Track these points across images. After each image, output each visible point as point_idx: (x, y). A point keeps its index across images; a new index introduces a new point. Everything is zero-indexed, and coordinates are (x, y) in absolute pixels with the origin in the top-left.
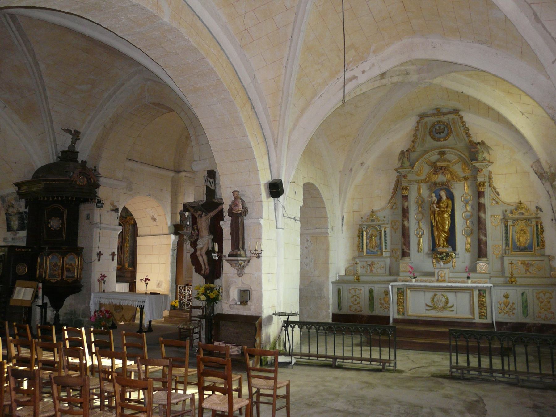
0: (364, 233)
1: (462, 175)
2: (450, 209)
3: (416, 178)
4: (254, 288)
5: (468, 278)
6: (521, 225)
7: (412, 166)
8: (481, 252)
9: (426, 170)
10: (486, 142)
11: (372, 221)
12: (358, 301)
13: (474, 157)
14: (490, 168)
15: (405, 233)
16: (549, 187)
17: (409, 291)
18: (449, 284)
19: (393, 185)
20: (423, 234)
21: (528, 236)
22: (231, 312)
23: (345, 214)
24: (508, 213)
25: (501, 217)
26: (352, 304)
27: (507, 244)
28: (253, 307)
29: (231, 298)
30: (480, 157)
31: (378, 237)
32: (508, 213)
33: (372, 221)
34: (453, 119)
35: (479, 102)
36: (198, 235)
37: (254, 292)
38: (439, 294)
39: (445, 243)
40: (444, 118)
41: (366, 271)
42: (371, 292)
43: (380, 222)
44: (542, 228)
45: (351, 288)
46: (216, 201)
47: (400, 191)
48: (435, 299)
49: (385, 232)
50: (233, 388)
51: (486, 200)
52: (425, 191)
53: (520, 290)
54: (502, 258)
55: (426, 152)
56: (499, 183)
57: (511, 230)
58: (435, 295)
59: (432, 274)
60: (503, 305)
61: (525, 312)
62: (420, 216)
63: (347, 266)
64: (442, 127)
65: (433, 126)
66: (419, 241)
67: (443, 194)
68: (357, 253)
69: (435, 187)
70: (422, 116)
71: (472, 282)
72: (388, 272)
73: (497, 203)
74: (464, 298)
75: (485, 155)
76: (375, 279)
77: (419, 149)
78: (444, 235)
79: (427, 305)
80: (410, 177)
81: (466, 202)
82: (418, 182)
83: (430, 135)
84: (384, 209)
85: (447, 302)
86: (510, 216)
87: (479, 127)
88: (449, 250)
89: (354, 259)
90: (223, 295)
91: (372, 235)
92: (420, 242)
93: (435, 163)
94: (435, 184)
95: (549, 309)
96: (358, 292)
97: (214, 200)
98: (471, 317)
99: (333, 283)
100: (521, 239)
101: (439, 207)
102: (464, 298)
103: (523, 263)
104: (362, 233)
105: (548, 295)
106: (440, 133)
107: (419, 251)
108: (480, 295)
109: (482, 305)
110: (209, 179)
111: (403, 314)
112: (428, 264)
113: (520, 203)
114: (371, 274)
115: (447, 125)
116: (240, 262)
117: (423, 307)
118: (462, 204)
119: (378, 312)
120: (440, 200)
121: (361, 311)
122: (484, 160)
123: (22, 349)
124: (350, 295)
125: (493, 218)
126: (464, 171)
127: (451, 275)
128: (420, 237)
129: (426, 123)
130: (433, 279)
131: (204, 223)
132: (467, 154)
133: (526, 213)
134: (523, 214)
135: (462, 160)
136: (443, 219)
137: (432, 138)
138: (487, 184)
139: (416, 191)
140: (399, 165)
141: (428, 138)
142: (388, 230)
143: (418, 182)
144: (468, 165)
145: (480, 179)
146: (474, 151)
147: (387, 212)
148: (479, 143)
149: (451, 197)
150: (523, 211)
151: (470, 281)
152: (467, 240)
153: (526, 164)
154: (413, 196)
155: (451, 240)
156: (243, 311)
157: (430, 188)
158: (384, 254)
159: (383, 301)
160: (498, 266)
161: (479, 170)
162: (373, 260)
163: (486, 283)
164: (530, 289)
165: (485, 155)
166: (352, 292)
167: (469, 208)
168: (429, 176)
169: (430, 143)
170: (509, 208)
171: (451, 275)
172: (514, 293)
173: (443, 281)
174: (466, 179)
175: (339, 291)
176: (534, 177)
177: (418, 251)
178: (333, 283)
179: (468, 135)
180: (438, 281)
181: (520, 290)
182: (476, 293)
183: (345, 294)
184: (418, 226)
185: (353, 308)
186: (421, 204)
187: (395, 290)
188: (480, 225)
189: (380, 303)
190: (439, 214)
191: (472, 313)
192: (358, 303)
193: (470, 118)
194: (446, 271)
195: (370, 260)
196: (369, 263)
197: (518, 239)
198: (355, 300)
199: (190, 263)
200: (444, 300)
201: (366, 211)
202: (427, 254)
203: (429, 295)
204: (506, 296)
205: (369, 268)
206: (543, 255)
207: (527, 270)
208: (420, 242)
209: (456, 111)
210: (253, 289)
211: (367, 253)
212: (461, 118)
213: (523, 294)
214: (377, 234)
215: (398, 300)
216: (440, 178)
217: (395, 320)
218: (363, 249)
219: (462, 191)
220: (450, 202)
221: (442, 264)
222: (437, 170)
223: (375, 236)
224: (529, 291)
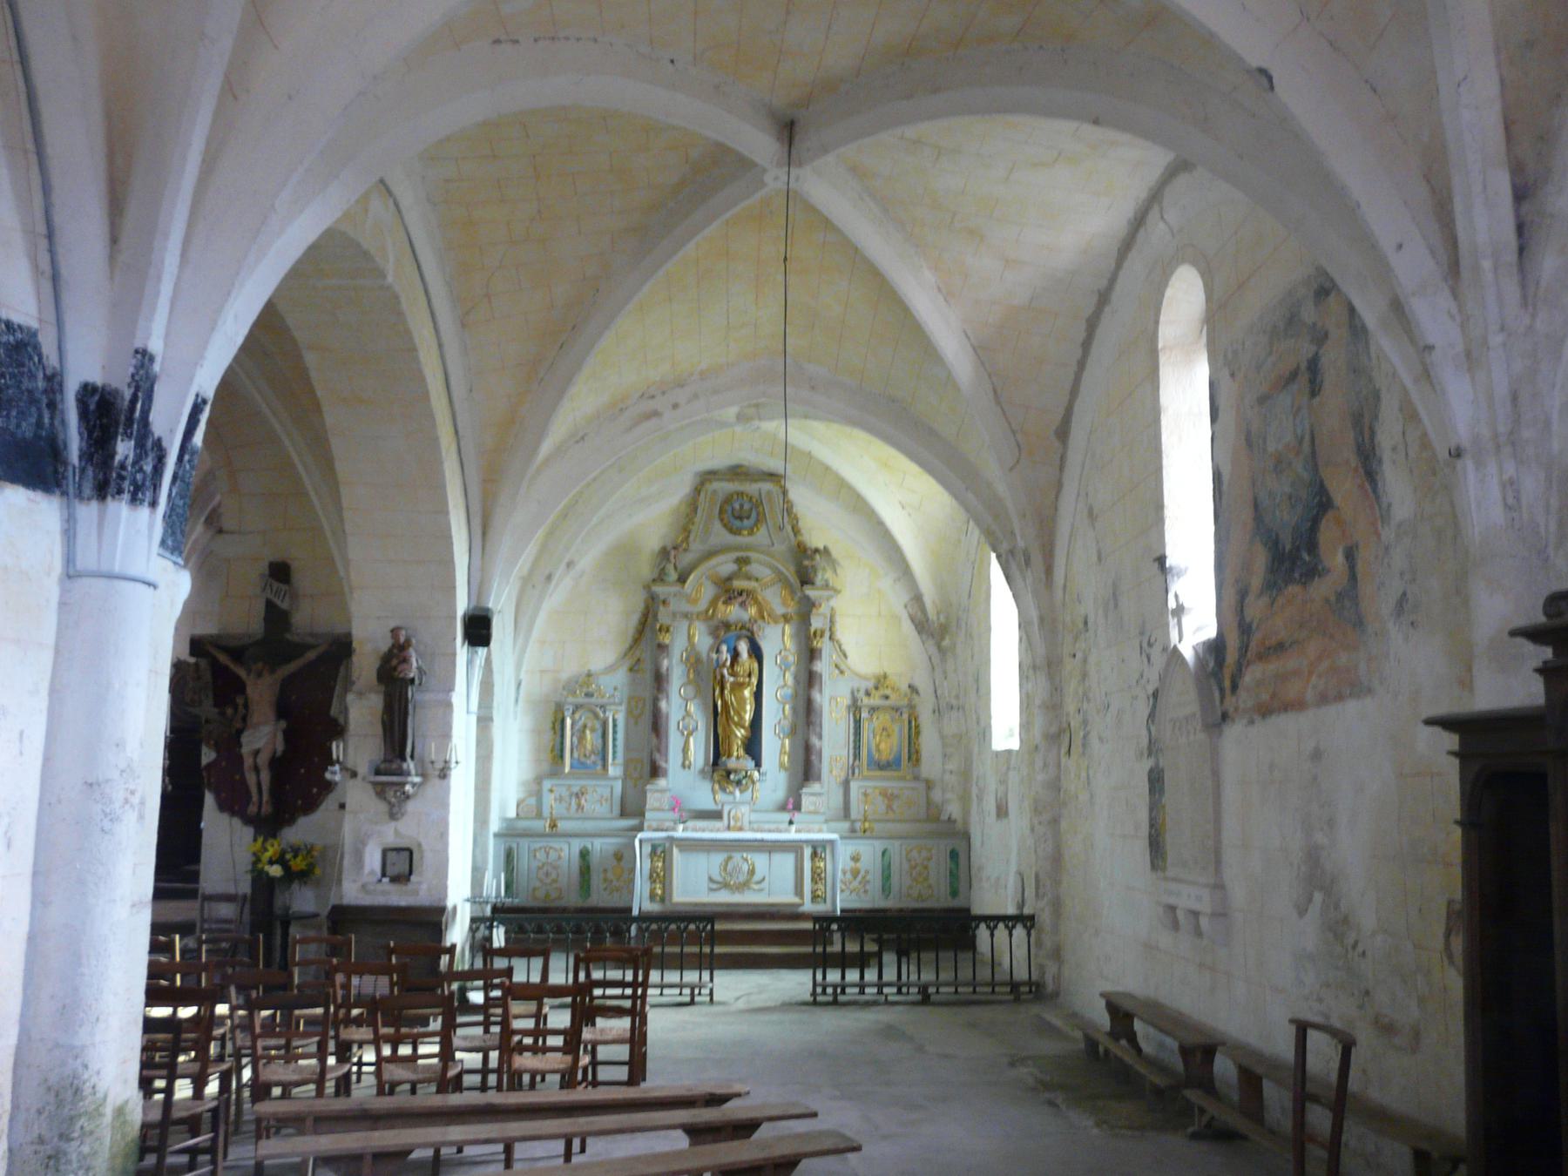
0: (568, 722)
1: (780, 610)
2: (754, 680)
3: (685, 607)
5: (791, 822)
6: (882, 719)
7: (682, 579)
8: (805, 768)
9: (708, 592)
10: (835, 553)
11: (588, 695)
12: (554, 876)
13: (806, 579)
14: (833, 603)
15: (657, 725)
16: (933, 650)
18: (759, 836)
19: (635, 619)
21: (895, 740)
22: (367, 900)
23: (523, 676)
24: (861, 694)
25: (847, 701)
26: (538, 884)
27: (857, 755)
28: (424, 886)
29: (367, 870)
30: (819, 580)
31: (600, 732)
32: (861, 694)
33: (588, 695)
34: (769, 493)
35: (827, 468)
36: (244, 719)
37: (428, 855)
38: (737, 857)
39: (742, 752)
40: (752, 488)
41: (568, 809)
42: (584, 854)
43: (605, 700)
44: (917, 727)
45: (537, 846)
46: (296, 639)
47: (647, 633)
48: (729, 867)
49: (614, 721)
51: (820, 666)
52: (703, 640)
53: (879, 845)
54: (846, 785)
55: (710, 554)
56: (848, 633)
57: (865, 725)
58: (730, 858)
59: (716, 815)
60: (849, 876)
61: (886, 889)
62: (691, 691)
63: (522, 796)
64: (747, 507)
65: (728, 500)
66: (687, 743)
67: (743, 647)
68: (546, 767)
69: (722, 630)
70: (708, 476)
71: (798, 831)
72: (617, 810)
73: (842, 672)
74: (784, 864)
75: (829, 575)
76: (589, 826)
77: (696, 547)
78: (740, 733)
79: (711, 880)
80: (674, 605)
81: (784, 668)
82: (686, 616)
83: (722, 520)
84: (610, 669)
85: (752, 872)
86: (866, 700)
87: (821, 522)
89: (539, 780)
90: (346, 862)
91: (585, 726)
92: (687, 744)
93: (729, 579)
94: (727, 626)
95: (926, 879)
96: (553, 855)
97: (288, 636)
98: (796, 900)
99: (496, 835)
100: (883, 746)
101: (733, 674)
102: (784, 864)
103: (884, 794)
104: (563, 721)
105: (924, 854)
106: (740, 518)
107: (685, 765)
108: (814, 854)
109: (817, 876)
110: (276, 585)
111: (663, 900)
112: (703, 795)
113: (885, 676)
114: (580, 814)
115: (757, 504)
117: (704, 884)
118: (777, 670)
119: (600, 897)
120: (735, 655)
121: (560, 898)
122: (826, 586)
124: (535, 864)
125: (832, 701)
126: (784, 604)
127: (754, 817)
128: (690, 734)
129: (715, 492)
130: (717, 824)
131: (261, 691)
132: (792, 568)
133: (893, 697)
134: (887, 697)
135: (781, 579)
136: (742, 701)
137: (725, 526)
138: (827, 634)
139: (685, 637)
140: (656, 575)
141: (717, 525)
142: (621, 718)
143: (686, 616)
145: (816, 623)
146: (805, 568)
147: (620, 678)
148: (816, 551)
149: (756, 653)
150: (888, 692)
151: (793, 827)
152: (783, 745)
153: (896, 599)
154: (678, 643)
155: (753, 747)
156: (397, 897)
157: (714, 632)
158: (611, 771)
159: (610, 875)
160: (837, 799)
162: (583, 782)
163: (820, 831)
164: (897, 843)
165: (829, 575)
166: (540, 855)
168: (713, 603)
169: (720, 535)
170: (864, 685)
171: (754, 817)
172: (869, 851)
173: (741, 829)
174: (786, 619)
175: (509, 856)
176: (908, 627)
177: (683, 766)
178: (496, 835)
179: (796, 531)
180: (729, 828)
181: (879, 845)
182: (807, 852)
183: (523, 863)
184: (683, 711)
185: (540, 894)
186: (694, 662)
187: (647, 849)
188: (806, 714)
189: (605, 880)
190: (732, 690)
191: (799, 890)
192: (555, 881)
193: (800, 495)
194: (745, 809)
195: (576, 785)
196: (576, 789)
197: (878, 746)
198: (547, 874)
200: (745, 867)
201: (570, 669)
202: (702, 772)
204: (856, 859)
205: (574, 801)
206: (916, 778)
207: (889, 807)
208: (687, 744)
209: (772, 476)
210: (425, 846)
211: (572, 767)
212: (785, 493)
213: (884, 853)
214: (598, 725)
215: (653, 870)
216: (733, 612)
217: (645, 918)
218: (562, 757)
219: (777, 642)
220: (756, 665)
221: (737, 793)
222: (728, 592)
223: (593, 730)
224: (895, 847)
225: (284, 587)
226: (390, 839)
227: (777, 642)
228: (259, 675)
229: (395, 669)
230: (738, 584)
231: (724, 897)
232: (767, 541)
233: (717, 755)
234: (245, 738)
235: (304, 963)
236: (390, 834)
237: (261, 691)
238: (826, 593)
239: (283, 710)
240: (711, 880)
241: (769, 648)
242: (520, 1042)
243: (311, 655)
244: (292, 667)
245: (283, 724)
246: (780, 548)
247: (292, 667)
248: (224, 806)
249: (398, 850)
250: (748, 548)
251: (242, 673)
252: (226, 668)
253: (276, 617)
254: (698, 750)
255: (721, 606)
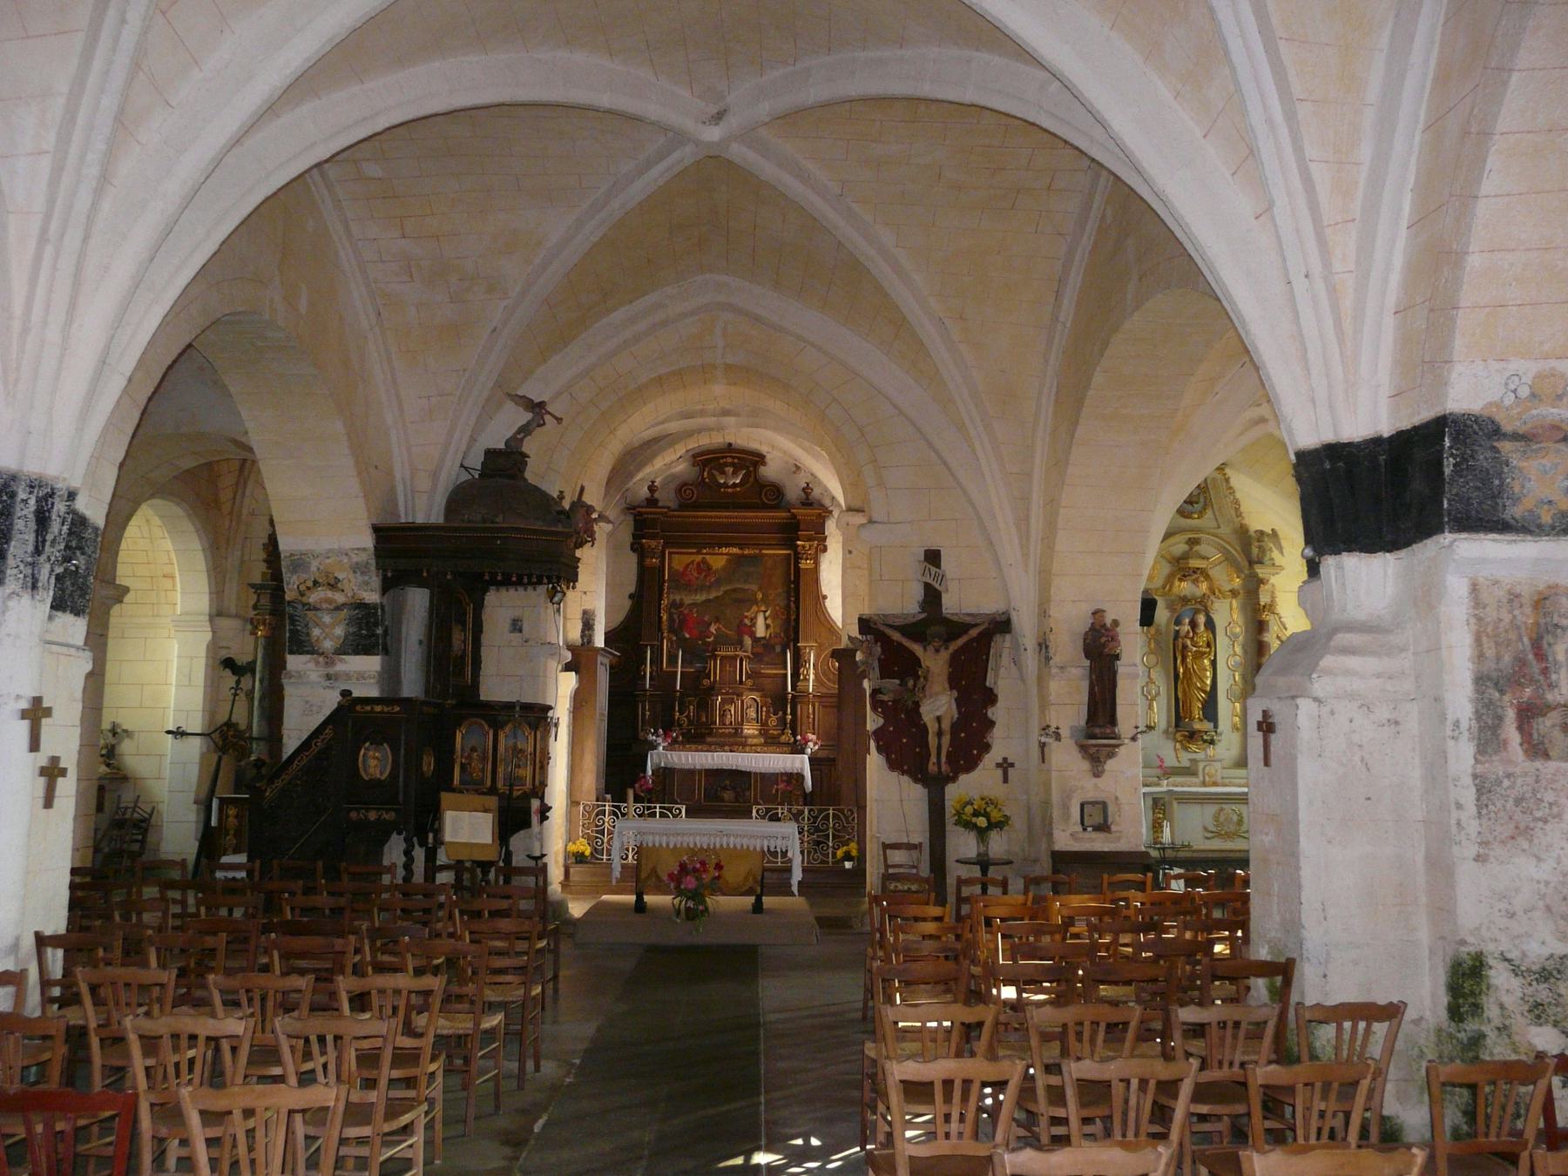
4: (1260, 842)
17: (1175, 804)
20: (1158, 694)
48: (1222, 819)
50: (610, 527)
67: (1201, 619)
79: (1206, 829)
81: (1233, 638)
88: (1208, 726)
94: (1185, 600)
111: (1103, 827)
112: (1171, 754)
116: (57, 971)
120: (1194, 625)
123: (438, 863)
130: (1194, 780)
131: (935, 662)
135: (1228, 558)
144: (1239, 570)
149: (1210, 625)
155: (1210, 709)
161: (1261, 581)
167: (1238, 649)
173: (1215, 784)
174: (1234, 593)
179: (1239, 514)
180: (1204, 784)
190: (1195, 658)
199: (730, 439)
200: (1235, 818)
202: (1166, 732)
203: (1211, 809)
210: (1122, 800)
212: (1227, 480)
225: (933, 569)
226: (1091, 795)
227: (1228, 615)
228: (937, 651)
229: (1104, 645)
230: (1195, 563)
231: (1217, 844)
232: (1214, 524)
233: (1178, 718)
234: (923, 710)
235: (174, 916)
236: (1090, 788)
237: (935, 662)
238: (1271, 570)
239: (953, 682)
240: (1206, 829)
241: (1220, 621)
242: (527, 985)
243: (974, 632)
244: (960, 642)
245: (955, 694)
246: (1225, 530)
247: (960, 642)
248: (895, 764)
249: (1094, 803)
250: (1198, 530)
251: (917, 648)
252: (900, 644)
253: (932, 597)
254: (1160, 713)
255: (1177, 583)
